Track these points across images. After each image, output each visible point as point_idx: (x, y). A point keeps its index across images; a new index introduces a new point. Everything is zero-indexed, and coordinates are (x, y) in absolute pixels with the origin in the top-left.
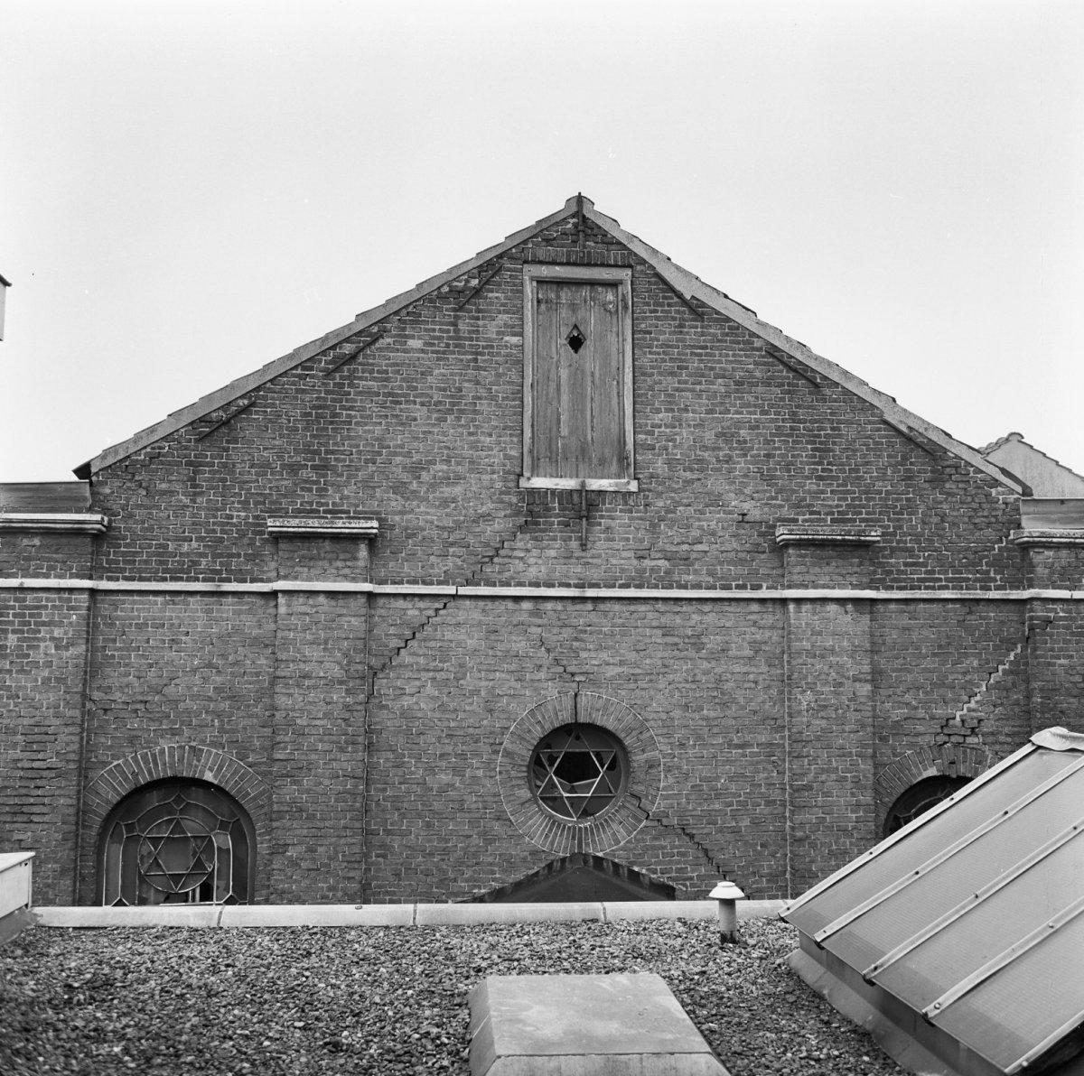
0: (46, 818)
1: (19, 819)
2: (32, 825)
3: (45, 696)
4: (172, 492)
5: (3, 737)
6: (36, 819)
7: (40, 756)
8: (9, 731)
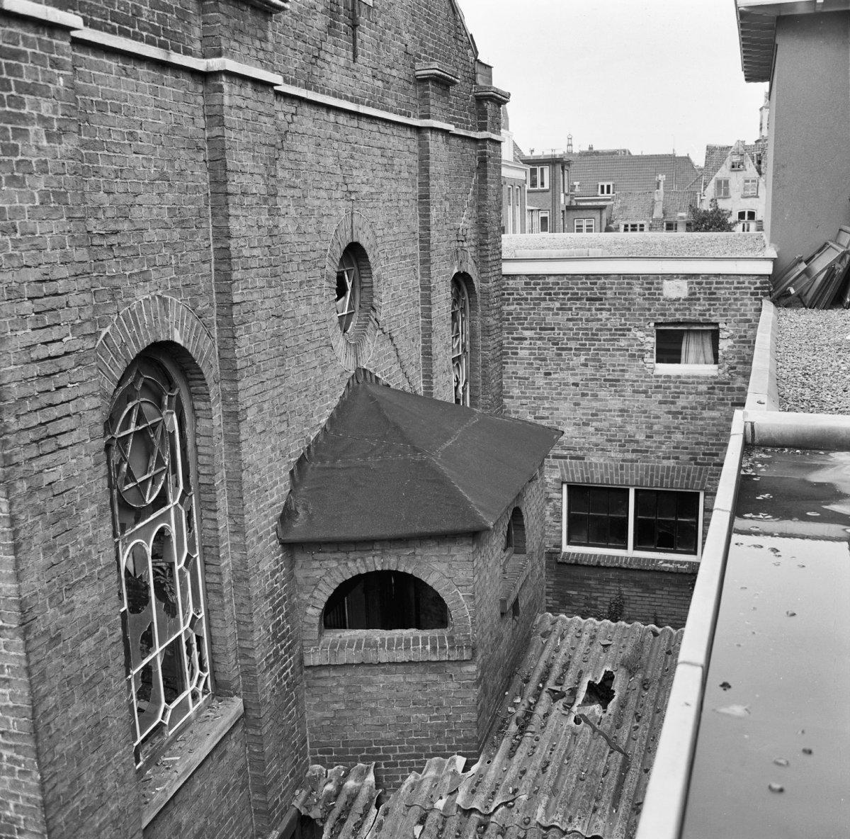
1: (47, 448)
5: (7, 306)
6: (63, 441)
8: (14, 295)
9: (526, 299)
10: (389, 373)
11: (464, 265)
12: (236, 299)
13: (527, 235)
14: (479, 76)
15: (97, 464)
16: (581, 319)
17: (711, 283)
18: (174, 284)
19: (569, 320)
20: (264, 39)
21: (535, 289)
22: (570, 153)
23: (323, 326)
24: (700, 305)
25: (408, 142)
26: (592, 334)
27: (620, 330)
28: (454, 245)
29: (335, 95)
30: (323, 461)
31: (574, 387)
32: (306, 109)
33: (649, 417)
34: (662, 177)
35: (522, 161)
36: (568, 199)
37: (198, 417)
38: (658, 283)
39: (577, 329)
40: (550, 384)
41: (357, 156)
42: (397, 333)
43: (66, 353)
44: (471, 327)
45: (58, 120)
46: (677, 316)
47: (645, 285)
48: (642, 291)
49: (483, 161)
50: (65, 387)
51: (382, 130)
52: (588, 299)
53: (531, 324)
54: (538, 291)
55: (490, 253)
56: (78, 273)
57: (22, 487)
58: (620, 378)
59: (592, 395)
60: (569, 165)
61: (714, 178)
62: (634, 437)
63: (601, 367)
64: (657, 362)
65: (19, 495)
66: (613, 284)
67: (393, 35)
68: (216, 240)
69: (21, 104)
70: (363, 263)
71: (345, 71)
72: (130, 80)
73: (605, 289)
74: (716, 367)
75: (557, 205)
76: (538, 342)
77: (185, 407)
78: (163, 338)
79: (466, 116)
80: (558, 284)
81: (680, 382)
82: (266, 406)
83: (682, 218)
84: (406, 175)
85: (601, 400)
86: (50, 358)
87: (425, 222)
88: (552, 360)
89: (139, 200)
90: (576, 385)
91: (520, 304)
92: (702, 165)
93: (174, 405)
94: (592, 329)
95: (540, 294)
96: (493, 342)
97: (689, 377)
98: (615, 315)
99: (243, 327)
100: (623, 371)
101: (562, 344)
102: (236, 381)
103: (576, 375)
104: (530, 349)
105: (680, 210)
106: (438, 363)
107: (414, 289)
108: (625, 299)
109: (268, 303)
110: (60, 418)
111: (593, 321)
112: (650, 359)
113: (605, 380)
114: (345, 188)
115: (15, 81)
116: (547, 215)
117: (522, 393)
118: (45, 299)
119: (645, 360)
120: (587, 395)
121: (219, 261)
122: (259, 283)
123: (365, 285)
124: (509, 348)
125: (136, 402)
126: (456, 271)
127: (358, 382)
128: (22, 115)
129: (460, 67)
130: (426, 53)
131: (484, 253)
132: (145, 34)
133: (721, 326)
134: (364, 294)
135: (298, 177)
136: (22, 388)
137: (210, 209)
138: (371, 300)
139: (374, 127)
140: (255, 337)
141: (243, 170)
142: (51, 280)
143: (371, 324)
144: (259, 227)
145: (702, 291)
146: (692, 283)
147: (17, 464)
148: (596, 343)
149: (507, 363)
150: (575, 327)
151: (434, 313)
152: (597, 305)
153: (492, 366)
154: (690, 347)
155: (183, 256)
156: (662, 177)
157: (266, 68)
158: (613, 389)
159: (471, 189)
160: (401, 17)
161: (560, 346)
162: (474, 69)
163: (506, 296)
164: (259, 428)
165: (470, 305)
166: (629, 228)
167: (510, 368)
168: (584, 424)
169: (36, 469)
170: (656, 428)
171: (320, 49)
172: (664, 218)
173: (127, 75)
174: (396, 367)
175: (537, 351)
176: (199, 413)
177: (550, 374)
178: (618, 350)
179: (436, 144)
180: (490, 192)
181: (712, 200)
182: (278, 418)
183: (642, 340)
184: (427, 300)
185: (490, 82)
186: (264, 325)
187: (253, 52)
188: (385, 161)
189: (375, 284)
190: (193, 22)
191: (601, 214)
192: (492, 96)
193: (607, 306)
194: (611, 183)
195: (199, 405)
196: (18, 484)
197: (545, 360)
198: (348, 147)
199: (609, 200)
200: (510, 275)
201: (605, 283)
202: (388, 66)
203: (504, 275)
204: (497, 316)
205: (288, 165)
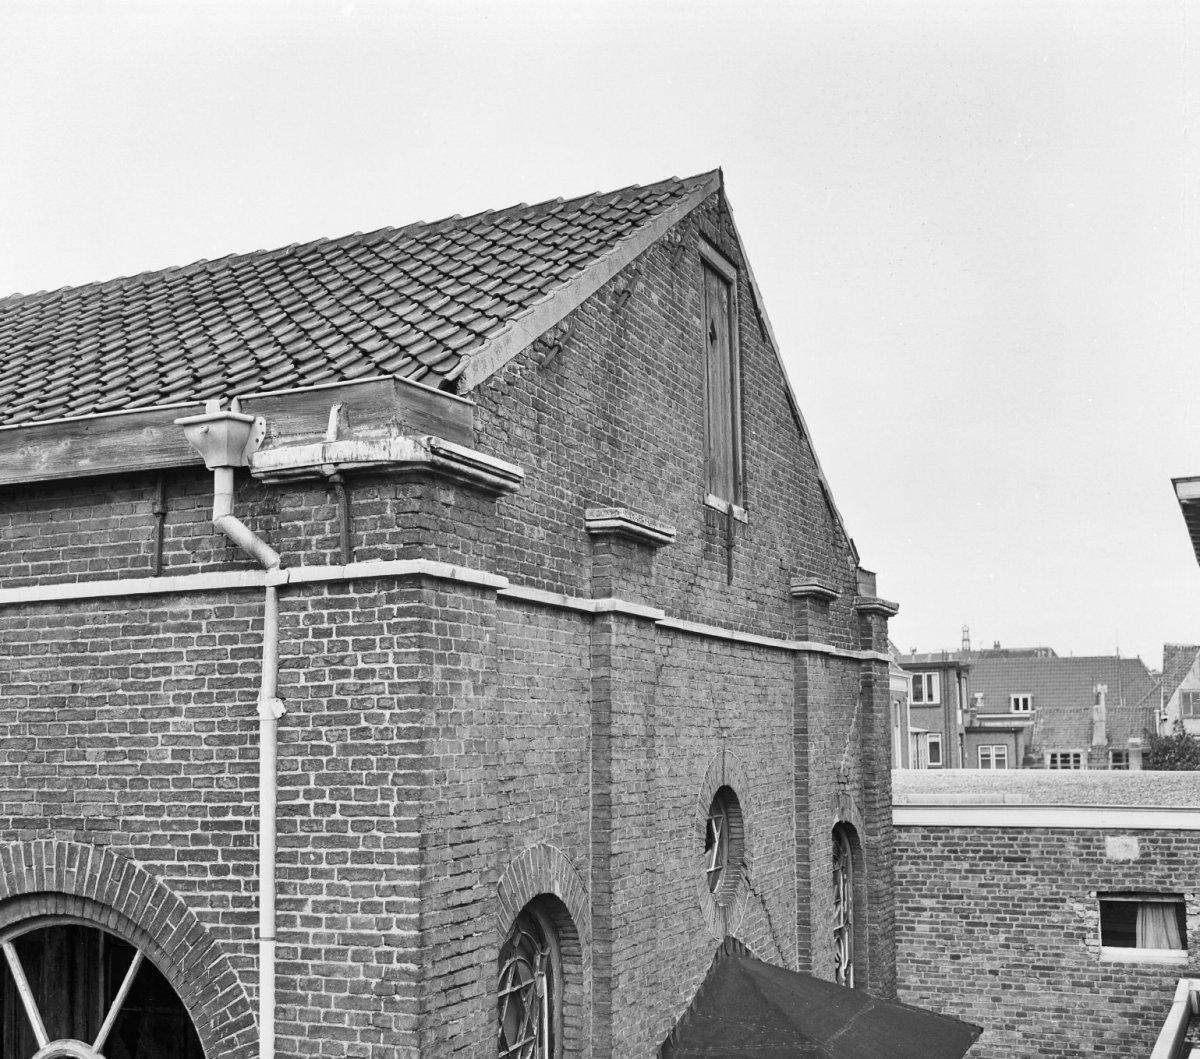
6: (467, 992)
7: (466, 881)
9: (925, 858)
10: (761, 947)
11: (847, 811)
12: (615, 850)
13: (911, 771)
14: (861, 585)
15: (491, 1021)
16: (998, 886)
17: (1170, 841)
18: (557, 832)
19: (982, 886)
20: (648, 575)
21: (935, 845)
22: (967, 652)
23: (691, 883)
24: (1156, 869)
25: (783, 668)
26: (1014, 905)
27: (1051, 900)
28: (834, 788)
29: (709, 622)
30: (691, 1048)
31: (992, 976)
32: (681, 641)
33: (1097, 1020)
34: (1102, 688)
35: (900, 665)
36: (968, 717)
37: (567, 983)
38: (1098, 840)
39: (993, 898)
40: (959, 971)
41: (730, 687)
42: (770, 895)
43: (475, 901)
44: (856, 892)
45: (484, 673)
46: (1127, 884)
47: (1082, 843)
48: (1077, 850)
49: (868, 685)
50: (471, 936)
51: (756, 656)
52: (1007, 859)
53: (932, 890)
54: (940, 847)
55: (878, 798)
56: (489, 819)
57: (431, 1036)
58: (1054, 965)
59: (1017, 987)
60: (967, 671)
61: (1177, 691)
62: (1078, 1047)
63: (1028, 950)
64: (1103, 945)
65: (428, 1046)
66: (1039, 839)
67: (767, 551)
68: (596, 785)
69: (457, 661)
70: (734, 810)
71: (719, 595)
72: (532, 627)
73: (1028, 846)
74: (1184, 953)
75: (952, 726)
76: (942, 914)
77: (554, 970)
78: (545, 890)
79: (847, 634)
80: (966, 839)
81: (1137, 973)
82: (637, 973)
83: (1135, 745)
84: (780, 706)
85: (1030, 995)
86: (462, 905)
87: (802, 761)
88: (960, 938)
89: (533, 745)
90: (994, 973)
91: (917, 864)
92: (1160, 670)
93: (544, 966)
94: (1013, 898)
95: (943, 852)
96: (883, 912)
97: (1148, 966)
98: (1043, 880)
99: (619, 881)
100: (1057, 955)
101: (974, 917)
102: (611, 942)
103: (994, 959)
104: (931, 923)
105: (1132, 733)
106: (817, 935)
107: (789, 841)
108: (1056, 860)
109: (644, 855)
110: (464, 968)
111: (1014, 888)
112: (1094, 941)
113: (1034, 967)
114: (717, 724)
115: (455, 640)
116: (938, 740)
117: (921, 981)
118: (462, 846)
119: (1087, 941)
120: (1010, 987)
121: (598, 808)
122: (636, 832)
123: (734, 836)
124: (902, 921)
125: (513, 959)
126: (836, 820)
127: (727, 954)
128: (458, 670)
129: (839, 577)
130: (802, 565)
131: (871, 798)
132: (546, 581)
133: (1187, 897)
134: (733, 847)
135: (671, 714)
136: (439, 935)
137: (591, 750)
138: (742, 854)
139: (747, 654)
140: (630, 893)
141: (625, 710)
142: (467, 827)
143: (741, 884)
144: (638, 771)
145: (1158, 851)
146: (1145, 840)
147: (429, 1012)
148: (1020, 917)
149: (900, 941)
150: (990, 896)
151: (813, 872)
152: (1019, 866)
153: (882, 943)
154: (1149, 926)
155: (565, 802)
156: (1102, 688)
157: (649, 603)
158: (1045, 979)
159: (854, 720)
160: (775, 529)
161: (970, 920)
162: (855, 578)
163: (898, 853)
164: (630, 999)
165: (853, 864)
166: (1059, 759)
167: (903, 948)
168: (1008, 1027)
169: (443, 1020)
170: (1107, 1035)
171: (696, 575)
172: (1109, 745)
173: (530, 623)
174: (769, 939)
175: (940, 926)
176: (568, 978)
177: (958, 957)
178: (1049, 927)
179: (815, 669)
180: (877, 722)
181: (1176, 722)
182: (648, 989)
183: (1082, 915)
184: (804, 856)
185: (874, 591)
186: (638, 879)
187: (638, 589)
188: (758, 691)
189: (746, 835)
190: (585, 564)
191: (1016, 739)
192: (878, 609)
193: (1032, 869)
194: (1028, 696)
195: (568, 967)
196: (429, 1034)
197: (951, 938)
198: (720, 678)
199: (1027, 719)
200: (902, 826)
201: (1028, 839)
202: (763, 585)
203: (894, 826)
204: (888, 879)
205: (663, 701)
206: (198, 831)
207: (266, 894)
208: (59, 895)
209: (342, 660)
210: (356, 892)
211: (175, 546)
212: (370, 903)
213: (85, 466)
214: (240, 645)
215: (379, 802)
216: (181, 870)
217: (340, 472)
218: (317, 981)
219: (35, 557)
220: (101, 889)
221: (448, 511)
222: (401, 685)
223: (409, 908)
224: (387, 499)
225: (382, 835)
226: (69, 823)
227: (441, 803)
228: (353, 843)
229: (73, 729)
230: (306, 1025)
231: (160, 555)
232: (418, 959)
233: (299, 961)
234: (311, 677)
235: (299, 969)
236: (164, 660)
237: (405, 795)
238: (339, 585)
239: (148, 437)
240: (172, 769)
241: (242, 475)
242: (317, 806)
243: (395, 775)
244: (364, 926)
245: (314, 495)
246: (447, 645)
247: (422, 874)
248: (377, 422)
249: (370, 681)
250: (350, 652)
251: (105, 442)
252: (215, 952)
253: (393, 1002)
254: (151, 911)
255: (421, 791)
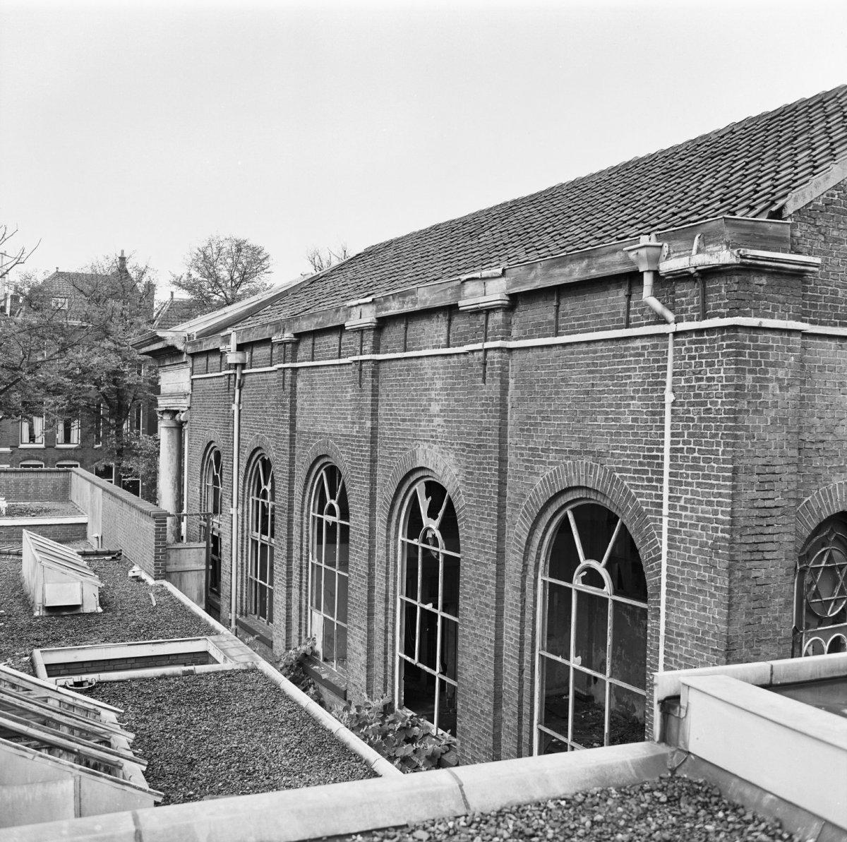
0: (774, 555)
2: (765, 562)
3: (773, 436)
4: (840, 240)
6: (768, 556)
7: (770, 495)
57: (739, 574)
147: (737, 561)
206: (641, 460)
207: (666, 493)
208: (586, 488)
209: (700, 373)
210: (703, 494)
211: (635, 312)
212: (709, 501)
213: (594, 273)
214: (661, 364)
215: (714, 448)
216: (633, 478)
217: (698, 271)
218: (685, 539)
219: (578, 319)
220: (602, 486)
221: (762, 289)
222: (727, 386)
223: (726, 505)
224: (721, 285)
225: (716, 465)
226: (590, 452)
227: (749, 451)
228: (702, 469)
229: (593, 406)
230: (680, 561)
231: (628, 317)
232: (731, 532)
233: (678, 528)
234: (687, 381)
235: (678, 532)
236: (629, 371)
237: (727, 444)
238: (699, 332)
239: (618, 257)
240: (631, 427)
241: (656, 273)
242: (688, 448)
243: (723, 434)
244: (707, 512)
245: (690, 284)
246: (758, 364)
247: (734, 487)
248: (716, 242)
249: (712, 383)
250: (704, 368)
251: (601, 260)
252: (647, 522)
253: (717, 553)
254: (622, 498)
255: (734, 443)
